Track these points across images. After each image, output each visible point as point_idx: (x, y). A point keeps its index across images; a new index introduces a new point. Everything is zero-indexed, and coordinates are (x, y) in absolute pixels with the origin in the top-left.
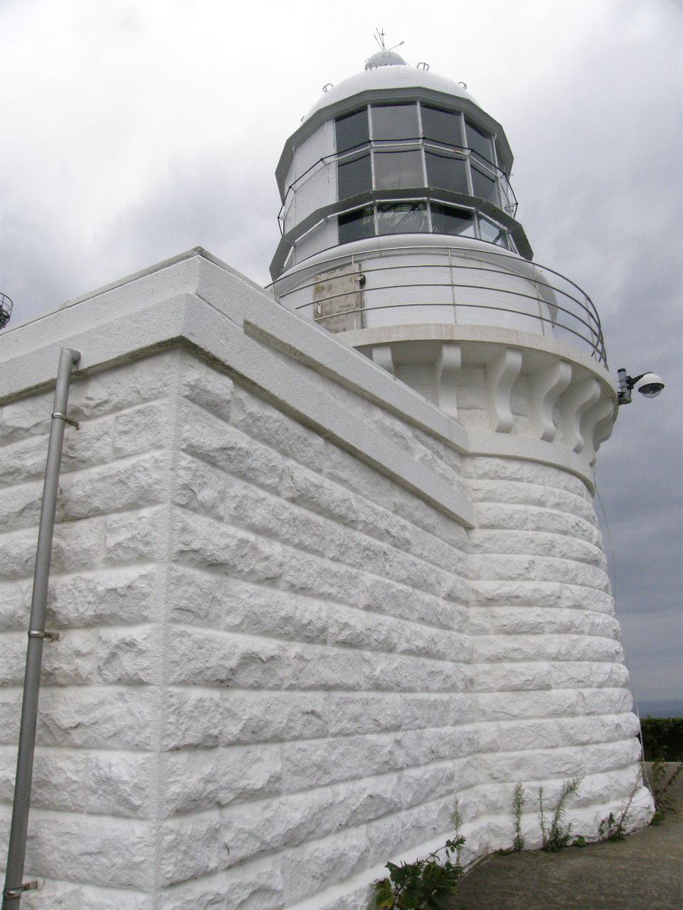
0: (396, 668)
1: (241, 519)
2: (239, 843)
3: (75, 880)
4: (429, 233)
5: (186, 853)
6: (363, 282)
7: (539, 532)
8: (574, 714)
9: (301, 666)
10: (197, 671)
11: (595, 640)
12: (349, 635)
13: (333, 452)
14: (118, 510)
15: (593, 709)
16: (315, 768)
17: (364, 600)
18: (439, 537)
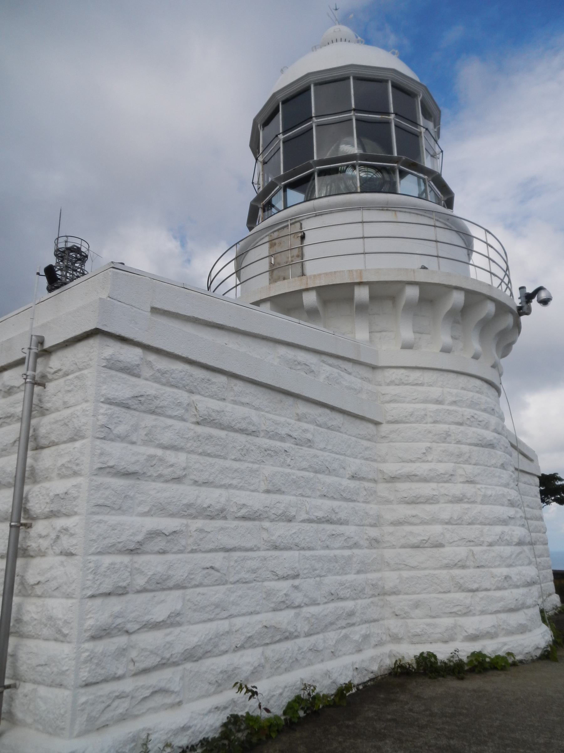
0: (295, 533)
1: (151, 441)
2: (143, 658)
5: (97, 664)
6: (303, 238)
8: (463, 567)
10: (110, 545)
12: (247, 512)
13: (235, 385)
15: (482, 564)
17: (263, 487)
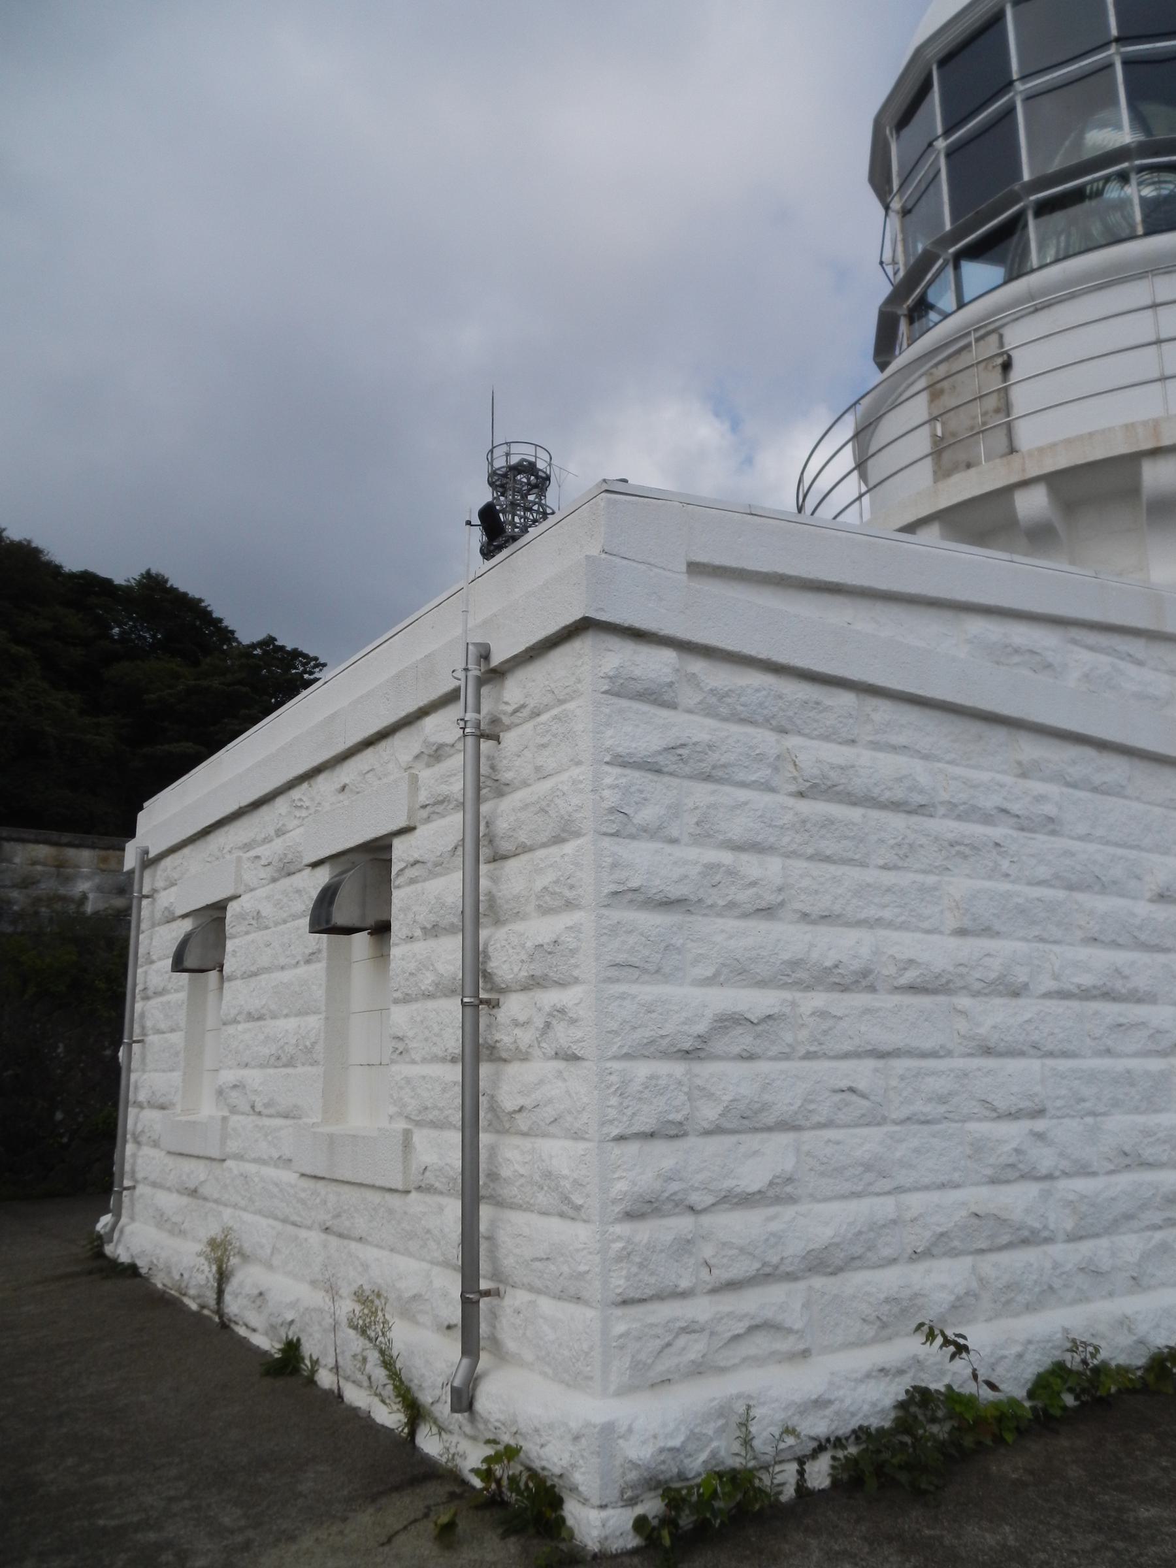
0: (1029, 1021)
2: (725, 1261)
3: (531, 1289)
5: (641, 1266)
6: (1007, 366)
9: (825, 1026)
10: (645, 1041)
14: (544, 845)
16: (861, 1169)
17: (951, 923)
18: (1138, 799)
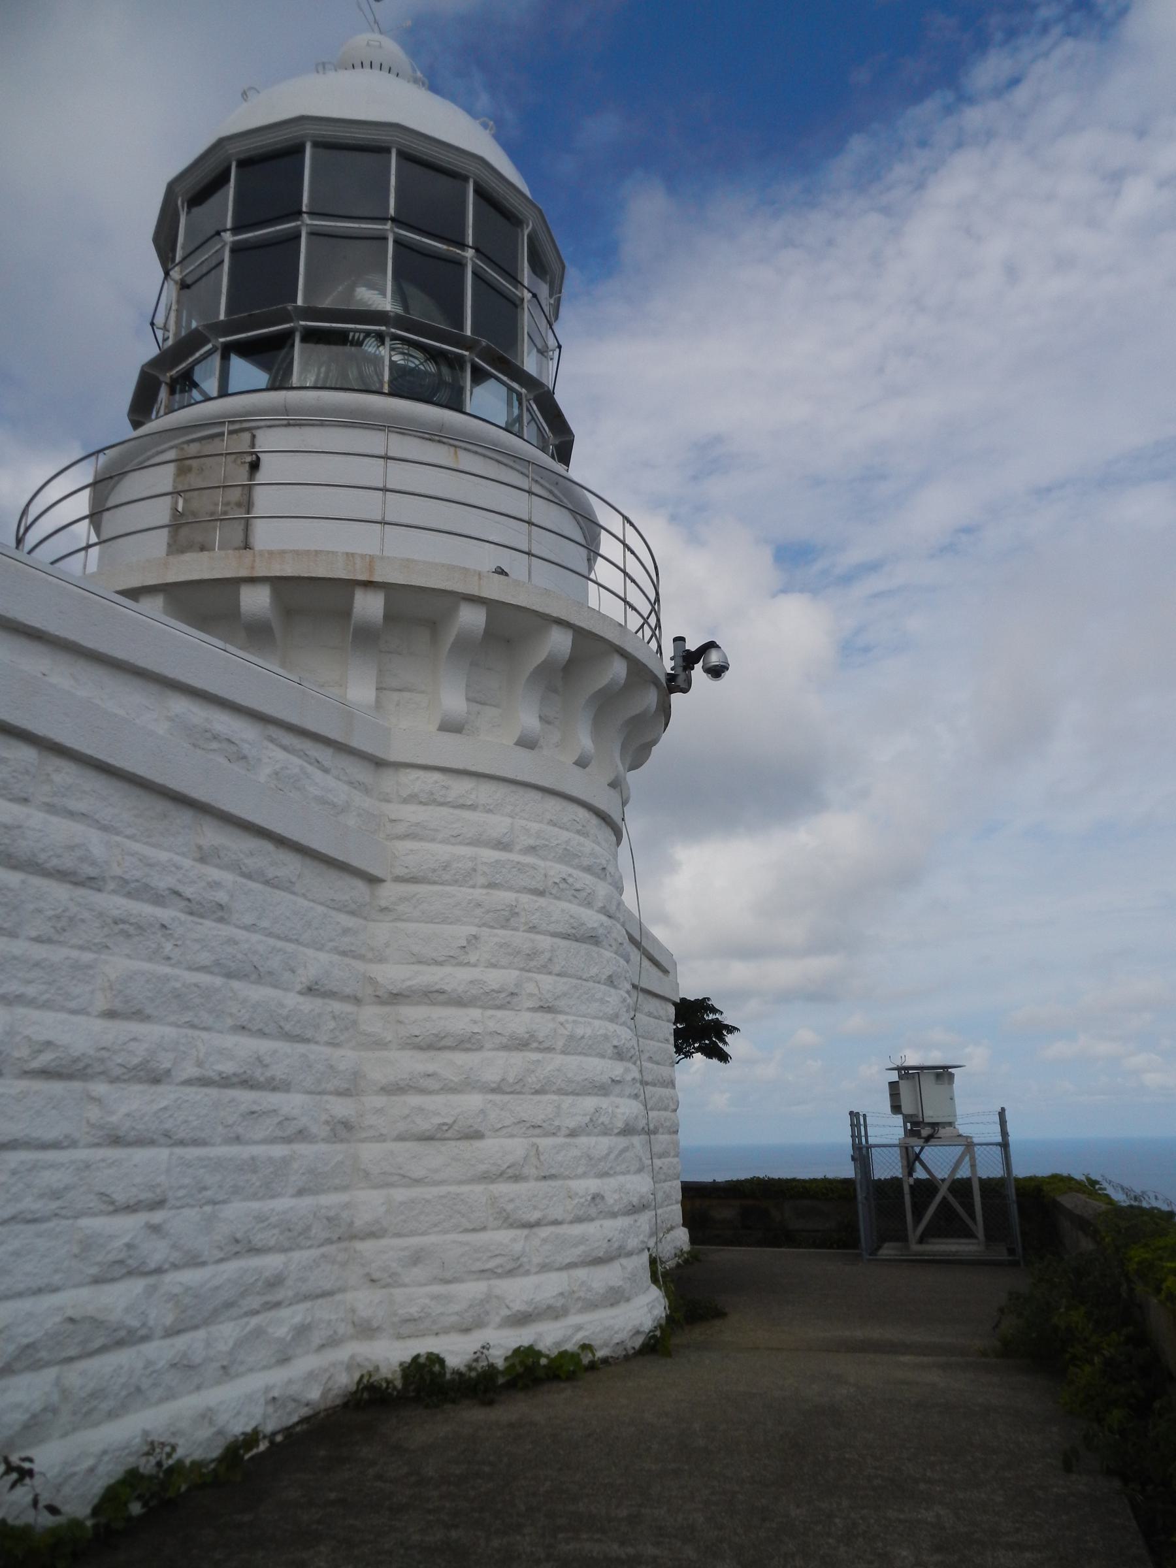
0: (165, 1108)
4: (379, 392)
6: (255, 466)
7: (491, 891)
8: (517, 1178)
11: (573, 1061)
15: (553, 1171)
18: (304, 896)
